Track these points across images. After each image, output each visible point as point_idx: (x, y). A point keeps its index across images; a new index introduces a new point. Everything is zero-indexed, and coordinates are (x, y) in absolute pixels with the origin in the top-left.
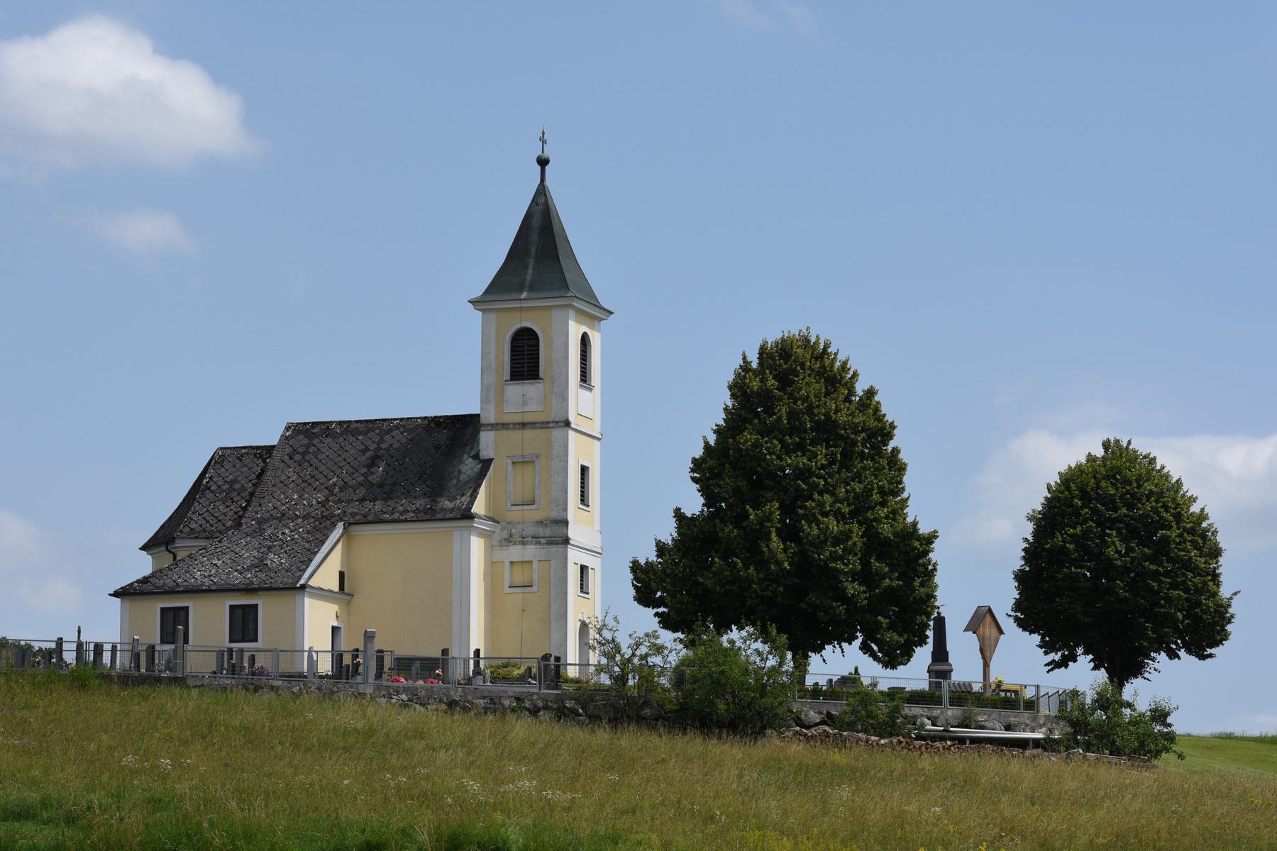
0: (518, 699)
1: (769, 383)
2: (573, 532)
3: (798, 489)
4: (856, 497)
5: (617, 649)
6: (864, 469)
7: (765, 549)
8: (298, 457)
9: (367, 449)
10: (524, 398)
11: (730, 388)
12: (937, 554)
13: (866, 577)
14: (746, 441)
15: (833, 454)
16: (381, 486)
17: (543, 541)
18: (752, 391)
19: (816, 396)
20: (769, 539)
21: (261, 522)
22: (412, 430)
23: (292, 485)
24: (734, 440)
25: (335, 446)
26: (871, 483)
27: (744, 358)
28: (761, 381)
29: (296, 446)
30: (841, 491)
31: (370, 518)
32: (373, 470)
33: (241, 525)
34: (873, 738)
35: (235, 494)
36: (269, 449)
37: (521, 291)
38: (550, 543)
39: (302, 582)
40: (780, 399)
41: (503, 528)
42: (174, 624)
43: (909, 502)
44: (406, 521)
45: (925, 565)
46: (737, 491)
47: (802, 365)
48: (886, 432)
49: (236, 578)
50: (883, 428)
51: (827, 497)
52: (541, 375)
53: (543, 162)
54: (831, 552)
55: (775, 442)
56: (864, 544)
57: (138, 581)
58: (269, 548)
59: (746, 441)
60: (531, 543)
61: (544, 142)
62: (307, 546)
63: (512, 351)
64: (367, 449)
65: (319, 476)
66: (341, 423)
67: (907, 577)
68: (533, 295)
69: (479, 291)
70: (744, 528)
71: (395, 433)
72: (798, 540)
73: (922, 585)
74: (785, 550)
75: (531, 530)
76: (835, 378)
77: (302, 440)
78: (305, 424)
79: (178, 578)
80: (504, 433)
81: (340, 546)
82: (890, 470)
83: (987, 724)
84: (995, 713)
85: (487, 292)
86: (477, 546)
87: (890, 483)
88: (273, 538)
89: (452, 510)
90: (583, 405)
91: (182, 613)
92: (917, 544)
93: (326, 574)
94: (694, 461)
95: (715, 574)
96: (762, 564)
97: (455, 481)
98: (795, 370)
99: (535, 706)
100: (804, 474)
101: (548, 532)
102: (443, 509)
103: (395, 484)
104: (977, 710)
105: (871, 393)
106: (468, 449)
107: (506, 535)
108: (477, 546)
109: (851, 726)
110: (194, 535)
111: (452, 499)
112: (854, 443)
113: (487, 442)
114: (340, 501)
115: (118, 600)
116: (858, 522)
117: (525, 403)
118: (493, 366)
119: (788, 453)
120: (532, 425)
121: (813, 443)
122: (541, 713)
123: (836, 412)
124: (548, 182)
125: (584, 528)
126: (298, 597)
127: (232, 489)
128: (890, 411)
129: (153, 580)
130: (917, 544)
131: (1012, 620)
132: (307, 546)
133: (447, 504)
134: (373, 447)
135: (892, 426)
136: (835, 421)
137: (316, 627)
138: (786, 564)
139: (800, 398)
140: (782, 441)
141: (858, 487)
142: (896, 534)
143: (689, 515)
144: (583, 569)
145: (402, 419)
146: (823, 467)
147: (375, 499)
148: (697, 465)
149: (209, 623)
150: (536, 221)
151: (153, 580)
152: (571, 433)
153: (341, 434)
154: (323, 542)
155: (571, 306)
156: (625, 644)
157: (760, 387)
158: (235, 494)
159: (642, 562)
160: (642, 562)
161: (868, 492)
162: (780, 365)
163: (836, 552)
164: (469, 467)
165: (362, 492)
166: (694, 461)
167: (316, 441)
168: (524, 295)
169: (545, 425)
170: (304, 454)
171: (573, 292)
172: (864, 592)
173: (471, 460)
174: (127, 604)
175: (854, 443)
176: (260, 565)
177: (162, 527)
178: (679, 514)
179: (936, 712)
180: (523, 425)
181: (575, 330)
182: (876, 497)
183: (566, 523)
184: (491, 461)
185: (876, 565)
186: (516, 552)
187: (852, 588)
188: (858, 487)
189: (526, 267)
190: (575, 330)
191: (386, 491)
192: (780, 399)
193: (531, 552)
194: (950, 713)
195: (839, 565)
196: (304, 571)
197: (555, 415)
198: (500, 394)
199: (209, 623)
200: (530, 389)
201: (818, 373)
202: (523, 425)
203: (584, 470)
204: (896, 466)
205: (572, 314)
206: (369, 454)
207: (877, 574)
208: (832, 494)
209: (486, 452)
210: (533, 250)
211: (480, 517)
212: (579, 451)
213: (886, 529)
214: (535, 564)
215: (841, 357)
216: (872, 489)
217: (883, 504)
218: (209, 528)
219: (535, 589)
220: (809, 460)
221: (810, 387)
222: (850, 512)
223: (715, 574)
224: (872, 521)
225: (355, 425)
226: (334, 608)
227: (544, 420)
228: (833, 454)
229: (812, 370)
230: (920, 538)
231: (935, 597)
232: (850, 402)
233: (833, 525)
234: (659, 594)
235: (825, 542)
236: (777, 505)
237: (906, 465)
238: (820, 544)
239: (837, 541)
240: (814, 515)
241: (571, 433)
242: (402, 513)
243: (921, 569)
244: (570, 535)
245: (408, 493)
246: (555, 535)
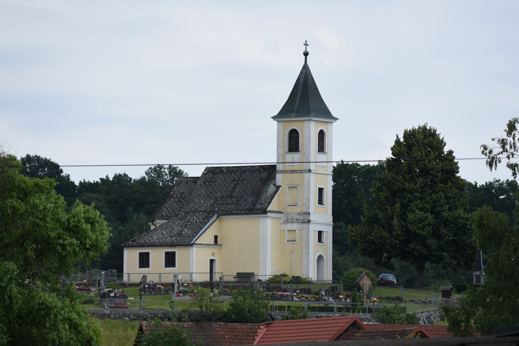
2: (312, 218)
8: (207, 183)
9: (234, 180)
11: (392, 149)
17: (300, 221)
21: (186, 213)
23: (202, 196)
27: (397, 137)
32: (235, 190)
35: (182, 199)
36: (197, 178)
38: (303, 223)
39: (192, 242)
41: (285, 216)
49: (169, 240)
52: (300, 150)
53: (306, 54)
58: (186, 225)
63: (289, 139)
69: (276, 113)
75: (295, 217)
77: (210, 175)
80: (285, 175)
89: (260, 209)
101: (302, 218)
102: (256, 209)
103: (242, 196)
106: (273, 181)
113: (279, 178)
114: (219, 204)
124: (308, 63)
126: (191, 248)
127: (181, 197)
150: (302, 81)
153: (226, 173)
154: (206, 223)
158: (182, 199)
164: (271, 189)
167: (215, 176)
170: (210, 182)
183: (309, 214)
184: (280, 186)
186: (290, 226)
193: (295, 226)
194: (336, 315)
200: (295, 156)
209: (278, 184)
210: (299, 94)
214: (297, 231)
225: (232, 169)
227: (301, 169)
242: (240, 211)
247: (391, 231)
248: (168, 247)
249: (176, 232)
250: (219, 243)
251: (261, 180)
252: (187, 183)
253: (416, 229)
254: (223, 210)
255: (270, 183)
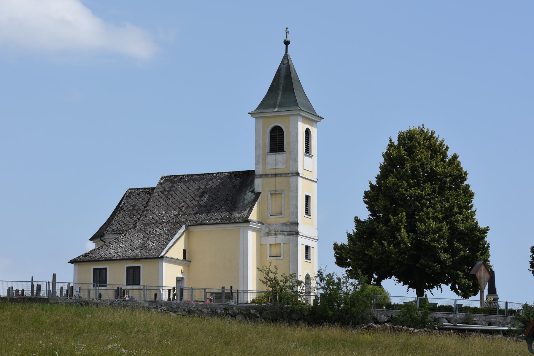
0: (225, 309)
1: (402, 153)
2: (301, 229)
3: (416, 206)
4: (446, 209)
5: (277, 282)
6: (451, 195)
7: (399, 237)
9: (200, 188)
10: (276, 161)
11: (384, 156)
12: (489, 238)
13: (451, 250)
14: (390, 182)
15: (434, 188)
16: (205, 206)
18: (393, 156)
19: (425, 159)
20: (400, 231)
21: (145, 225)
22: (223, 179)
23: (162, 207)
24: (384, 181)
25: (184, 187)
26: (453, 202)
27: (390, 141)
28: (398, 151)
29: (165, 187)
30: (438, 207)
31: (199, 223)
32: (202, 199)
33: (136, 227)
34: (411, 329)
36: (153, 189)
37: (275, 108)
40: (407, 160)
41: (266, 227)
42: (100, 277)
43: (476, 213)
44: (216, 224)
45: (483, 245)
46: (385, 207)
47: (419, 143)
48: (461, 177)
49: (130, 253)
50: (461, 175)
51: (430, 210)
52: (285, 149)
53: (287, 43)
54: (432, 238)
55: (404, 182)
56: (450, 233)
57: (82, 256)
59: (390, 182)
60: (280, 234)
61: (287, 33)
62: (167, 237)
63: (270, 138)
64: (200, 188)
65: (176, 202)
66: (188, 176)
67: (474, 250)
68: (281, 109)
69: (254, 107)
70: (389, 226)
71: (214, 180)
72: (415, 232)
73: (481, 255)
74: (408, 237)
75: (280, 228)
76: (436, 149)
77: (169, 184)
78: (170, 176)
79: (103, 253)
81: (183, 236)
82: (465, 196)
83: (478, 322)
84: (483, 317)
85: (258, 108)
86: (252, 237)
87: (464, 202)
88: (151, 233)
90: (306, 165)
91: (104, 271)
92: (478, 233)
93: (176, 251)
94: (365, 193)
95: (374, 249)
96: (397, 245)
97: (242, 204)
98: (415, 146)
99: (234, 313)
100: (419, 198)
101: (288, 229)
102: (235, 218)
103: (212, 205)
104: (472, 315)
105: (455, 157)
106: (249, 188)
107: (266, 229)
108: (252, 237)
109: (403, 323)
110: (114, 232)
111: (239, 213)
112: (445, 182)
113: (258, 184)
114: (185, 214)
115: (72, 265)
116: (446, 222)
117: (277, 164)
118: (261, 146)
119: (411, 188)
120: (280, 175)
121: (424, 182)
122: (237, 317)
123: (436, 167)
124: (289, 53)
125: (307, 227)
128: (465, 166)
129: (90, 255)
130: (478, 233)
131: (531, 272)
132: (167, 237)
133: (237, 215)
134: (203, 187)
135: (466, 174)
136: (435, 171)
137: (170, 275)
138: (409, 244)
139: (417, 160)
140: (407, 182)
141: (447, 205)
142: (467, 228)
143: (362, 220)
144: (307, 248)
145: (218, 173)
146: (429, 195)
147: (202, 213)
148: (367, 195)
149: (117, 275)
150: (283, 73)
151: (90, 255)
152: (300, 179)
153: (188, 181)
154: (174, 235)
155: (299, 115)
156: (280, 279)
157: (397, 155)
159: (339, 244)
160: (339, 244)
161: (452, 207)
162: (408, 143)
163: (434, 238)
164: (249, 196)
165: (196, 209)
166: (365, 193)
167: (175, 185)
168: (276, 110)
169: (287, 175)
170: (169, 191)
171: (301, 107)
172: (450, 258)
173: (250, 193)
174: (77, 267)
175: (445, 182)
176: (143, 247)
177: (100, 229)
178: (357, 220)
179: (451, 316)
180: (276, 175)
181: (302, 127)
182: (456, 209)
184: (260, 193)
185: (456, 244)
186: (272, 239)
187: (444, 256)
188: (447, 205)
189: (277, 95)
190: (302, 127)
191: (208, 209)
192: (407, 160)
193: (280, 239)
194: (458, 316)
195: (436, 244)
196: (163, 249)
197: (291, 170)
198: (265, 159)
199: (117, 275)
200: (279, 157)
201: (428, 147)
202: (276, 175)
203: (307, 198)
204: (469, 195)
205: (300, 118)
206: (200, 191)
207: (457, 249)
208: (434, 208)
209: (257, 190)
210: (281, 87)
211: (253, 222)
212: (304, 188)
213: (462, 226)
214: (282, 246)
215: (440, 139)
216: (454, 205)
217: (460, 213)
218: (121, 229)
219: (282, 258)
220: (422, 191)
221: (422, 154)
222: (442, 218)
223: (374, 249)
224: (454, 222)
225: (195, 177)
226: (180, 268)
228: (434, 188)
229: (425, 146)
230: (479, 230)
231: (488, 261)
232: (445, 162)
233: (433, 224)
234: (349, 260)
235: (429, 232)
236: (404, 214)
237: (474, 193)
238: (426, 233)
239: (435, 232)
240: (423, 219)
241: (300, 179)
243: (481, 246)
244: (299, 230)
245: (218, 210)
246: (292, 230)
247: (397, 245)
248: (131, 261)
249: (137, 245)
250: (187, 259)
251: (234, 187)
252: (139, 195)
253: (430, 241)
254: (191, 221)
255: (246, 190)
